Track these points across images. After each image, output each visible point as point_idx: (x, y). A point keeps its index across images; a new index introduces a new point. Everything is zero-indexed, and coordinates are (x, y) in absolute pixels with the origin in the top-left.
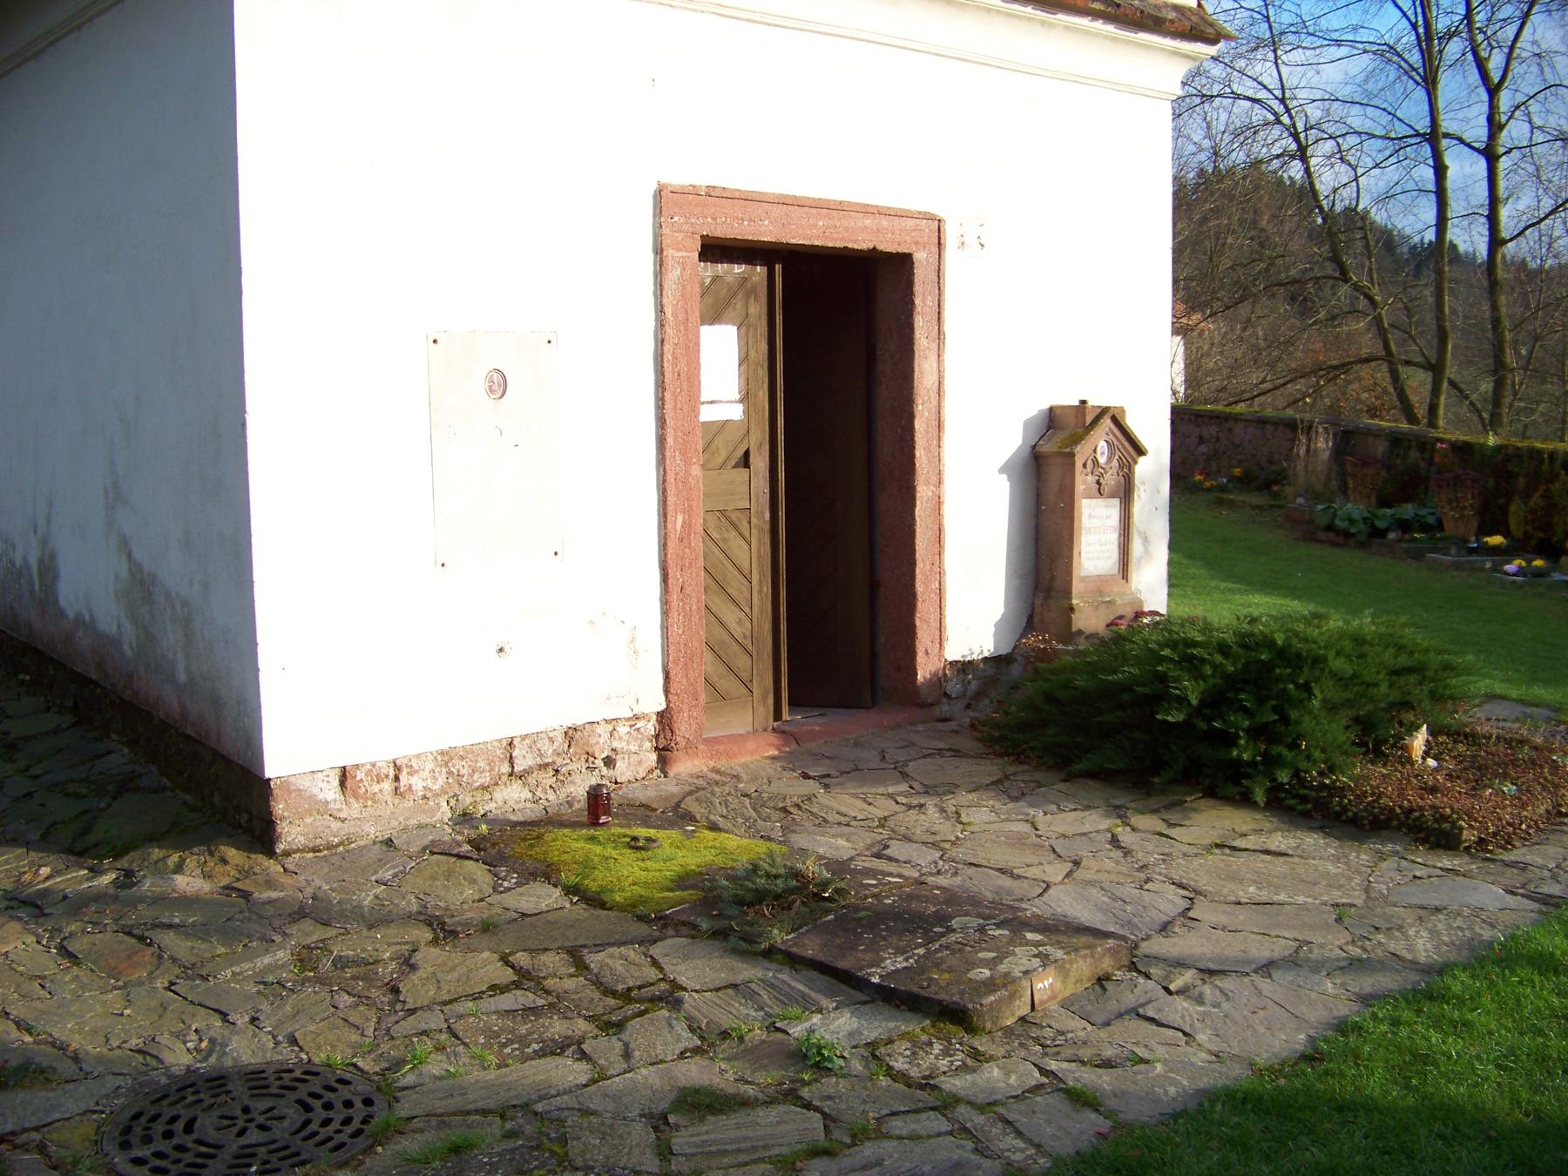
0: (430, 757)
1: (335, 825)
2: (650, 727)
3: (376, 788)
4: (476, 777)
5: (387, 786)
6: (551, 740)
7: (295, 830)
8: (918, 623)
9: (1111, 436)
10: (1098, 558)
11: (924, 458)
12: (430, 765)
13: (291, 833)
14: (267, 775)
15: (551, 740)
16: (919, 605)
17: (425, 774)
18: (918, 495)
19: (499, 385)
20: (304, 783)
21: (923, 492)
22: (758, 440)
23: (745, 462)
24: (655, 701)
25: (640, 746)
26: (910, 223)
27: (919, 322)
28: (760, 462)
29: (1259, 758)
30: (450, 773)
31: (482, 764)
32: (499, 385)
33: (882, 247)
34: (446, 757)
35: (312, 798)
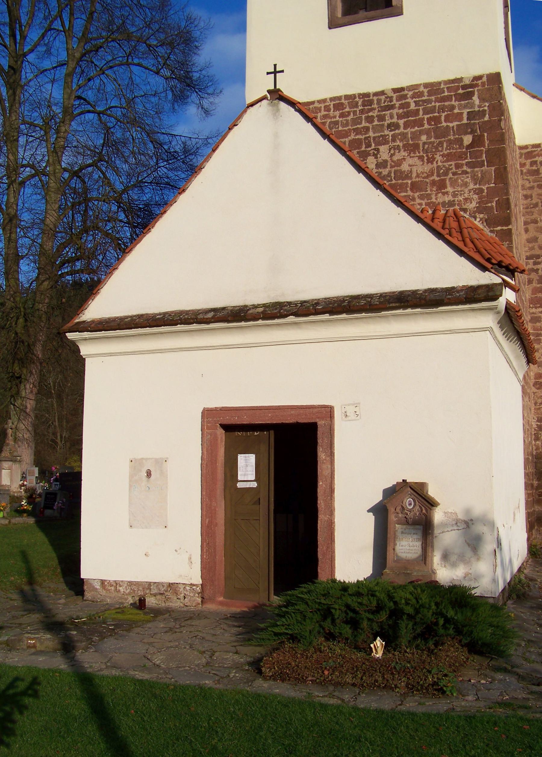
0: (126, 583)
1: (99, 596)
2: (199, 589)
3: (110, 588)
4: (139, 592)
5: (113, 588)
6: (163, 586)
7: (89, 595)
8: (319, 571)
9: (413, 496)
10: (408, 553)
11: (322, 504)
12: (125, 585)
13: (88, 595)
14: (82, 577)
15: (163, 586)
16: (320, 563)
17: (124, 587)
18: (319, 519)
19: (149, 474)
20: (92, 582)
21: (322, 517)
22: (263, 495)
23: (258, 502)
24: (201, 582)
25: (194, 595)
26: (316, 410)
27: (320, 450)
28: (264, 503)
29: (427, 636)
30: (131, 589)
31: (141, 589)
32: (149, 474)
33: (300, 421)
34: (131, 583)
35: (93, 587)
